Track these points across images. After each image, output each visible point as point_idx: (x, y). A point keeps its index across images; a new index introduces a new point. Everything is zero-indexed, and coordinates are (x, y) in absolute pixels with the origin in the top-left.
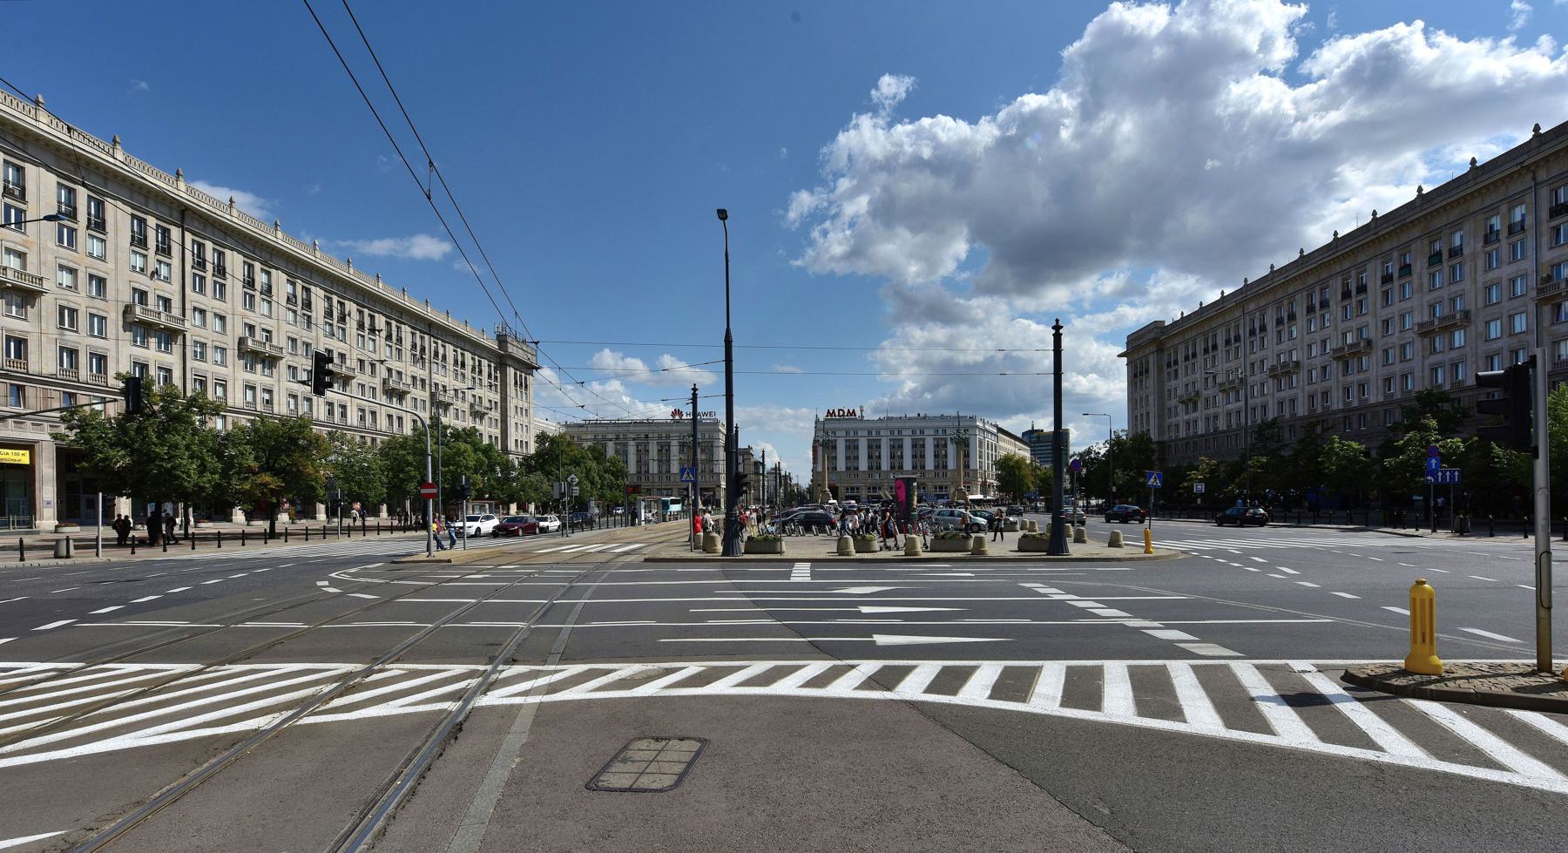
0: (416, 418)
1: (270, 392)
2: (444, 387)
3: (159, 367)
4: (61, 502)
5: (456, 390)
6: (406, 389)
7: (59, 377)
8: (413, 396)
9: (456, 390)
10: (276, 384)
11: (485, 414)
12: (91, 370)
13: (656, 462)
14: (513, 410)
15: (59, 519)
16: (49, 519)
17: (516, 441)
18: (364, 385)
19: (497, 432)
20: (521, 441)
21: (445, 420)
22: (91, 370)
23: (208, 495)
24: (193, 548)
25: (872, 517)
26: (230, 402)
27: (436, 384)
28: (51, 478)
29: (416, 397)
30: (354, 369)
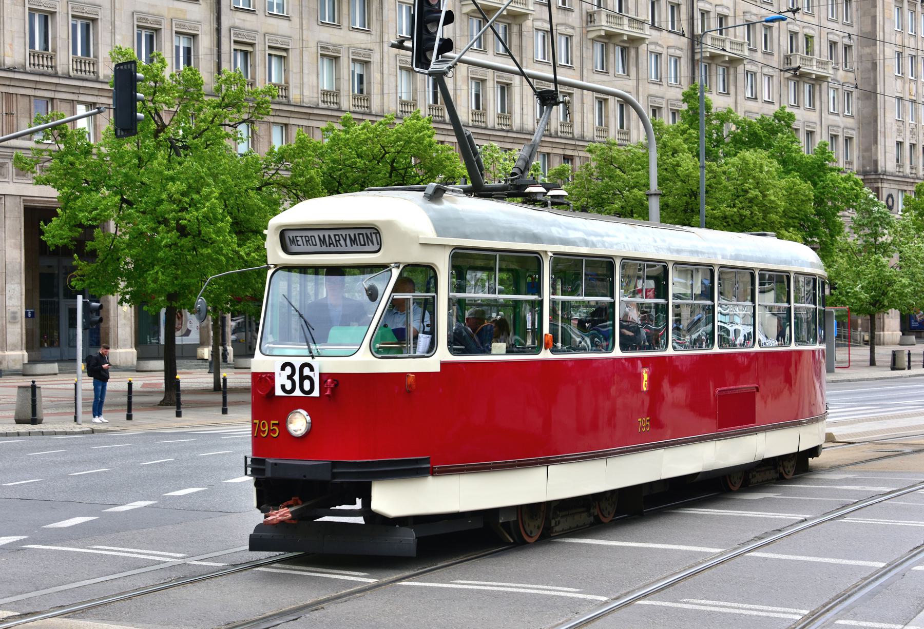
0: (480, 73)
1: (366, 63)
2: (722, 18)
3: (177, 33)
4: (32, 313)
5: (750, 25)
6: (636, 33)
7: (71, 74)
8: (652, 48)
9: (750, 25)
10: (376, 48)
11: (635, 41)
12: (75, 52)
13: (878, 92)
14: (891, 65)
15: (29, 347)
16: (125, 346)
17: (899, 144)
18: (755, 73)
19: (845, 123)
20: (912, 146)
21: (718, 102)
22: (75, 52)
23: (113, 290)
24: (129, 417)
25: (647, 333)
26: (294, 95)
27: (704, 13)
28: (18, 267)
29: (659, 49)
30: (742, 44)
